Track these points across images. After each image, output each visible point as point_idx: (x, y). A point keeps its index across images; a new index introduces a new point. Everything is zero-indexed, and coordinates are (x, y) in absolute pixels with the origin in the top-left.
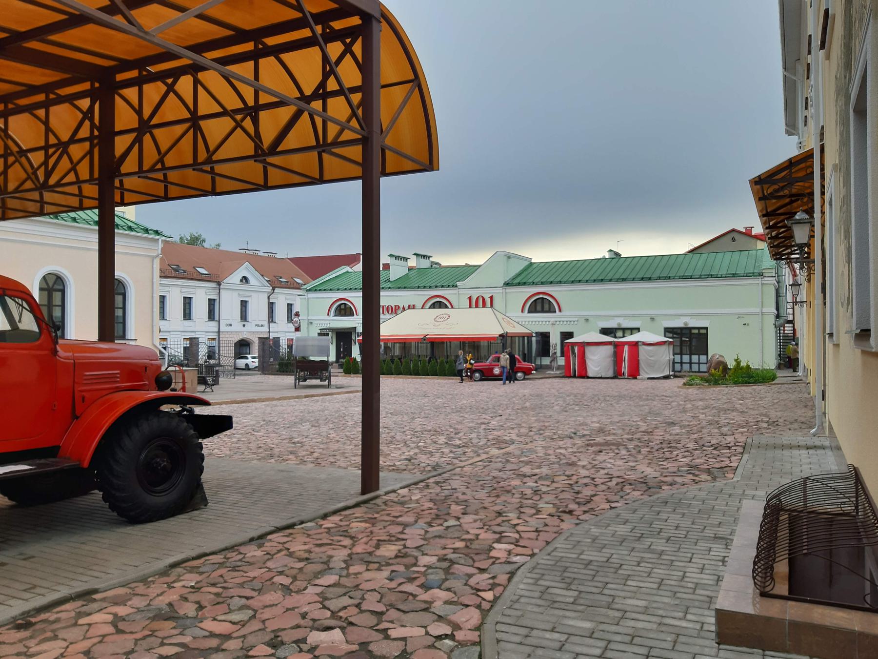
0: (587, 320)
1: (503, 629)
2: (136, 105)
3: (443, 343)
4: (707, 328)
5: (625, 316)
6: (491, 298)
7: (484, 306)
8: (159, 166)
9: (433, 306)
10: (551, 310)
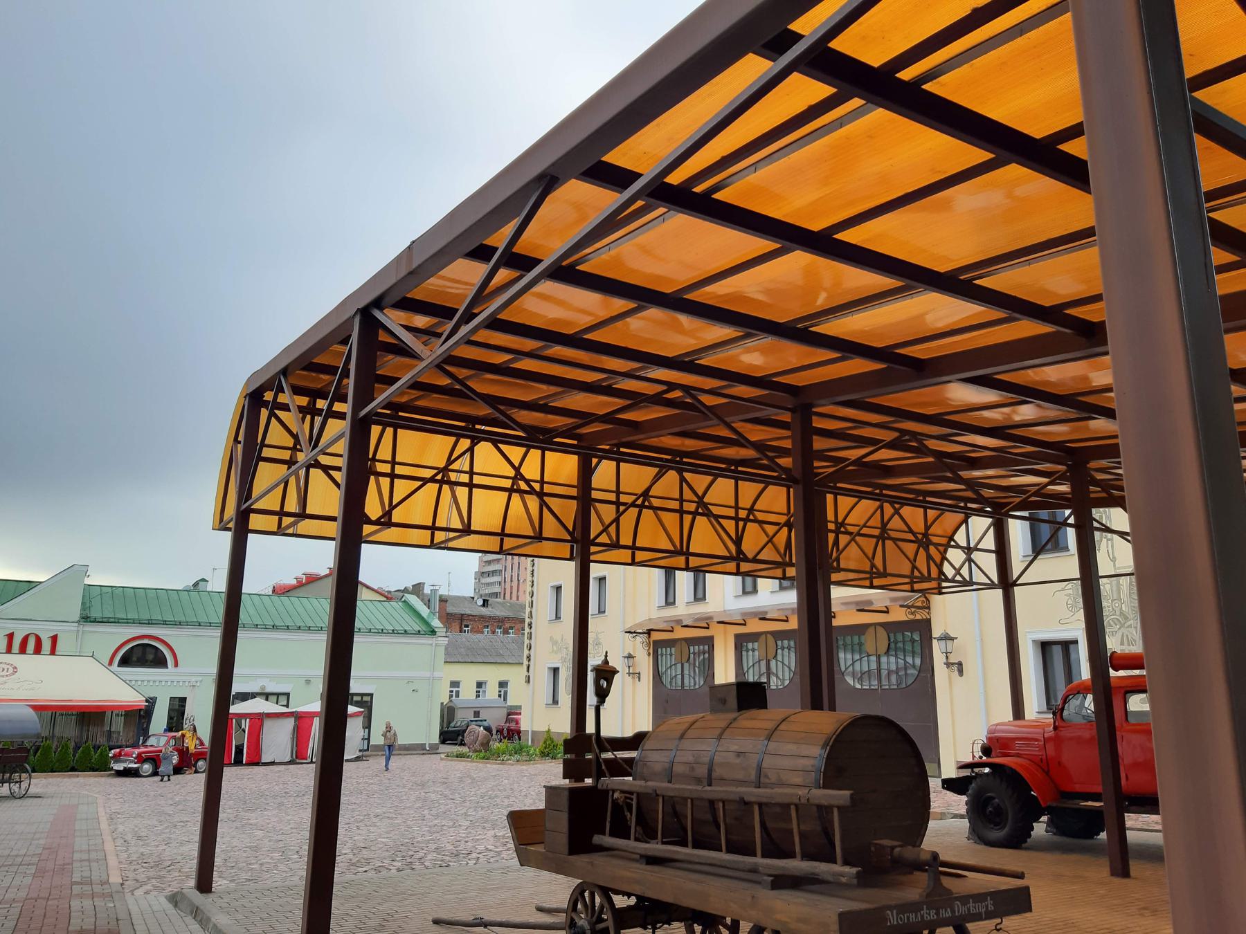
0: (308, 682)
4: (371, 695)
5: (271, 677)
6: (54, 639)
7: (38, 650)
8: (622, 508)
10: (160, 662)
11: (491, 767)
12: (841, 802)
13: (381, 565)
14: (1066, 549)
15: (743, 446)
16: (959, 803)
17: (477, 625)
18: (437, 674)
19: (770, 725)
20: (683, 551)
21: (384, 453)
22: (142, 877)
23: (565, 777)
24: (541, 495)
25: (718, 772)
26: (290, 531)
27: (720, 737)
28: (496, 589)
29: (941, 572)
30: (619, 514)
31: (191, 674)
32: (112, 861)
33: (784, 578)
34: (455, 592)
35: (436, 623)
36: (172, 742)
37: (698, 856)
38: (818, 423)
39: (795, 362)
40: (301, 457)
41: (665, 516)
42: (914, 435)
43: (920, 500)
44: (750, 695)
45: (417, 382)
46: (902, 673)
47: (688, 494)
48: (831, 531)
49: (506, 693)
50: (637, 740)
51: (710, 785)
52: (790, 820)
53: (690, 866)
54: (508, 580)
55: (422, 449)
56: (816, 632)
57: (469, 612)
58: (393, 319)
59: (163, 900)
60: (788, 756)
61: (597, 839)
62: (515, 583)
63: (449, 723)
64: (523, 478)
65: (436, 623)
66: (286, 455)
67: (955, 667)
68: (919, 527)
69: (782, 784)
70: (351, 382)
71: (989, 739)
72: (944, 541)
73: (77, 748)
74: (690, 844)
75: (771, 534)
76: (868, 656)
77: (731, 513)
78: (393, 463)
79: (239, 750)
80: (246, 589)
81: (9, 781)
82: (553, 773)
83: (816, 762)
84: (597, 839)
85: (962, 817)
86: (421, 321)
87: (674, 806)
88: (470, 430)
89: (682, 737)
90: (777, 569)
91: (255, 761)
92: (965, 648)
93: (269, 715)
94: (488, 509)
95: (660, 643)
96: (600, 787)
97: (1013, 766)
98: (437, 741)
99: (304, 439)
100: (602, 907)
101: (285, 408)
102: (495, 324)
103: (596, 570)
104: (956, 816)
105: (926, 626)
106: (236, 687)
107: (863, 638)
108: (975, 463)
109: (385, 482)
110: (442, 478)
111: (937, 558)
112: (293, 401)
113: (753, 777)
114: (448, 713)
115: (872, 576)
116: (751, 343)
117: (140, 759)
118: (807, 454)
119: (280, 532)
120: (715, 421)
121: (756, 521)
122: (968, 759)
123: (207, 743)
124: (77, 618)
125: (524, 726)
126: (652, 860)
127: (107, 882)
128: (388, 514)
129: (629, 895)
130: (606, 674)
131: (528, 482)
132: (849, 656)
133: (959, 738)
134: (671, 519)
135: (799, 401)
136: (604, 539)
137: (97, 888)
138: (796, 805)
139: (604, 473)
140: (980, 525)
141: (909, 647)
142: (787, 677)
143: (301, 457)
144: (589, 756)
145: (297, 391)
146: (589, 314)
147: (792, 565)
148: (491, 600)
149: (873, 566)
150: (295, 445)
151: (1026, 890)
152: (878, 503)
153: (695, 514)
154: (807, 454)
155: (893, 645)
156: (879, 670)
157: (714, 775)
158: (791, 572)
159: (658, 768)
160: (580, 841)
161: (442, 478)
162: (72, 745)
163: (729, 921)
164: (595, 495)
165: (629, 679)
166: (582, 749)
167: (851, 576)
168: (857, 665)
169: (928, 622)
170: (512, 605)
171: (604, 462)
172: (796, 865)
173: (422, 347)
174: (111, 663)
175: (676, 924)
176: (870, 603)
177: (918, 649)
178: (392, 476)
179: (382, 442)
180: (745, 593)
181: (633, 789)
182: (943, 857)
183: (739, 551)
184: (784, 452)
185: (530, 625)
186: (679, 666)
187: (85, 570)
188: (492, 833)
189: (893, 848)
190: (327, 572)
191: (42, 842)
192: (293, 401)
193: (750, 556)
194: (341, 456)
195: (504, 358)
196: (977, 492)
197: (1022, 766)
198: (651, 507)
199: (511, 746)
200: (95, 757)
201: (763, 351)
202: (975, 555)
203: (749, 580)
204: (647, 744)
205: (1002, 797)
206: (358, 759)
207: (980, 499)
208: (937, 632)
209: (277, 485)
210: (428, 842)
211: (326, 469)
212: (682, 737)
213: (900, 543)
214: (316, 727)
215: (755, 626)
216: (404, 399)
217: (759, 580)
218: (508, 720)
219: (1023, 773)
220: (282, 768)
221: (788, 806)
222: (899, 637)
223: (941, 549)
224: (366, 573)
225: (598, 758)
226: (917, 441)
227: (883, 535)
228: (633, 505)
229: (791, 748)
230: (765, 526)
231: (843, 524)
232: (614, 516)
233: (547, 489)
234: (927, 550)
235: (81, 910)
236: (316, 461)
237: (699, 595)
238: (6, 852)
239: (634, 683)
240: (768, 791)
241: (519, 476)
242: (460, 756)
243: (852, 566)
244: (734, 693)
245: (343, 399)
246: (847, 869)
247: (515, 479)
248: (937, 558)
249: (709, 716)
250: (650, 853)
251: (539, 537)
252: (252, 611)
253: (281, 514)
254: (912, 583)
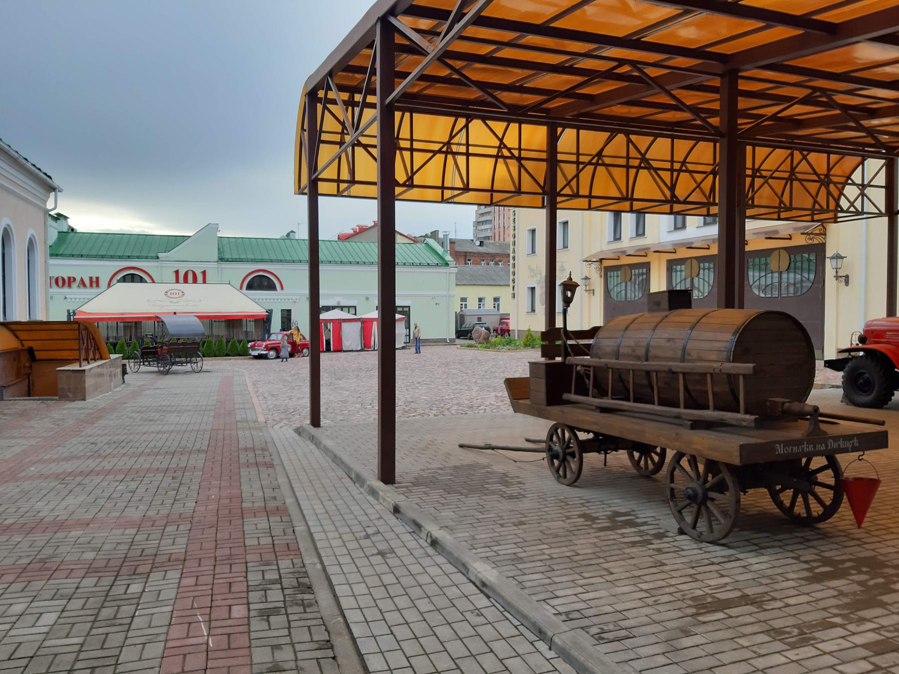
0: (367, 299)
1: (222, 652)
2: (523, 171)
3: (241, 320)
6: (204, 273)
7: (195, 281)
9: (124, 279)
10: (271, 287)
11: (490, 354)
12: (746, 372)
13: (410, 216)
15: (680, 110)
16: (837, 377)
17: (478, 258)
18: (451, 293)
19: (693, 320)
20: (628, 197)
21: (405, 133)
22: (277, 418)
23: (543, 356)
24: (519, 159)
25: (653, 352)
26: (346, 194)
27: (655, 328)
28: (489, 234)
29: (838, 205)
30: (579, 171)
31: (292, 294)
32: (258, 410)
33: (708, 215)
34: (460, 237)
35: (448, 258)
36: (286, 338)
37: (638, 408)
38: (743, 86)
39: (725, 33)
40: (348, 139)
41: (614, 170)
42: (824, 91)
43: (825, 146)
44: (678, 299)
45: (423, 75)
46: (798, 285)
47: (633, 153)
48: (749, 176)
49: (498, 305)
50: (593, 332)
51: (647, 360)
52: (706, 384)
53: (631, 414)
54: (497, 227)
55: (430, 128)
56: (732, 256)
57: (471, 250)
58: (404, 23)
59: (291, 431)
60: (709, 340)
61: (566, 396)
62: (502, 230)
63: (461, 325)
64: (505, 147)
65: (448, 258)
66: (337, 138)
67: (843, 279)
68: (822, 169)
69: (701, 360)
70: (377, 78)
71: (866, 331)
72: (842, 180)
73: (228, 342)
74: (632, 400)
75: (699, 181)
76: (772, 273)
77: (667, 165)
78: (412, 140)
79: (328, 342)
80: (321, 237)
81: (190, 362)
82: (536, 355)
83: (728, 344)
84: (566, 396)
85: (838, 387)
86: (425, 23)
87: (620, 375)
88: (467, 110)
89: (626, 329)
90: (703, 207)
91: (339, 350)
92: (854, 266)
93: (345, 321)
94: (481, 172)
95: (609, 268)
96: (567, 362)
97: (883, 351)
98: (454, 337)
99: (348, 125)
100: (570, 439)
101: (334, 102)
102: (480, 20)
103: (562, 216)
104: (833, 387)
105: (820, 249)
106: (323, 303)
107: (769, 260)
108: (874, 113)
109: (407, 154)
110: (447, 149)
111: (836, 193)
112: (339, 96)
113: (679, 353)
114: (460, 319)
115: (780, 211)
116: (688, 19)
117: (268, 348)
118: (732, 113)
119: (339, 194)
120: (658, 90)
121: (687, 171)
122: (847, 346)
123: (308, 337)
124: (216, 259)
125: (512, 327)
126: (604, 410)
127: (257, 421)
128: (411, 178)
129: (588, 432)
130: (570, 286)
131: (509, 150)
132: (757, 274)
133: (840, 332)
134: (619, 173)
135: (726, 66)
136: (567, 191)
137: (252, 425)
138: (711, 374)
139: (567, 138)
140: (874, 166)
141: (805, 266)
142: (707, 291)
143: (348, 139)
144: (558, 343)
145: (341, 88)
146: (554, 5)
147: (715, 204)
148: (486, 242)
149: (781, 202)
150: (343, 131)
151: (885, 434)
152: (789, 151)
153: (638, 168)
154: (732, 113)
155: (792, 265)
156: (780, 283)
157: (650, 354)
158: (714, 210)
159: (609, 350)
160: (554, 397)
161: (447, 149)
162: (224, 340)
163: (658, 450)
164: (560, 157)
165: (586, 294)
166: (553, 338)
167: (763, 211)
168: (763, 280)
169: (823, 245)
170: (500, 245)
171: (567, 130)
172: (710, 414)
173: (427, 44)
174: (241, 288)
175: (621, 451)
176: (776, 232)
177: (813, 267)
178: (412, 150)
179: (402, 122)
180: (676, 228)
181: (591, 364)
182: (821, 410)
183: (673, 195)
184: (713, 113)
185: (514, 258)
186: (624, 284)
187: (214, 227)
188: (493, 394)
189: (783, 403)
190: (373, 224)
191: (215, 398)
192: (339, 96)
193: (682, 199)
194: (375, 137)
195: (489, 48)
196: (875, 138)
197: (890, 350)
198: (604, 164)
199: (503, 340)
200: (240, 347)
201: (699, 25)
202: (868, 191)
203: (679, 217)
204: (600, 334)
205: (872, 373)
206: (403, 348)
207: (879, 144)
208: (829, 253)
209: (334, 160)
210: (452, 399)
211: (365, 147)
212: (626, 329)
213: (804, 183)
214: (375, 329)
215: (683, 254)
216: (415, 90)
217: (688, 217)
218: (501, 323)
219: (891, 356)
220: (356, 353)
221: (705, 374)
222: (798, 258)
223: (840, 186)
224: (400, 225)
225: (565, 344)
226: (829, 97)
227: (792, 177)
228: (590, 163)
229: (709, 335)
230: (695, 175)
231: (758, 170)
232: (575, 173)
233: (524, 154)
234: (827, 187)
235: (245, 438)
236: (358, 141)
237: (640, 231)
238: (196, 403)
239: (590, 298)
240: (690, 364)
241: (502, 145)
242: (470, 346)
243: (764, 203)
244: (666, 296)
245: (373, 93)
246: (748, 417)
247: (499, 148)
248: (836, 193)
249: (647, 314)
250: (603, 405)
251: (518, 191)
252: (326, 252)
253: (338, 181)
254: (812, 215)
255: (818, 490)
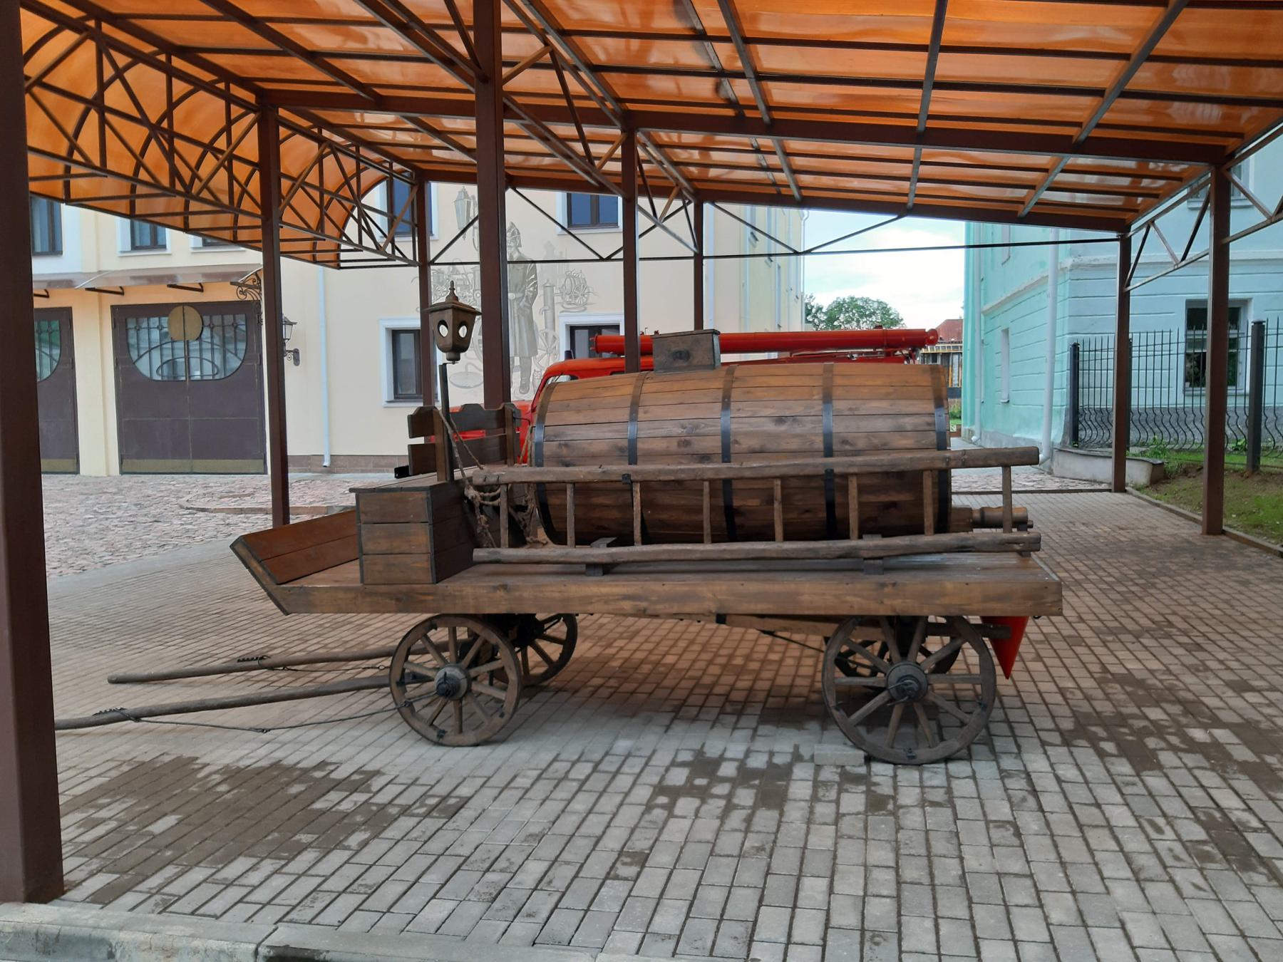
14: (616, 225)
76: (173, 342)
157: (734, 448)
255: (530, 650)
